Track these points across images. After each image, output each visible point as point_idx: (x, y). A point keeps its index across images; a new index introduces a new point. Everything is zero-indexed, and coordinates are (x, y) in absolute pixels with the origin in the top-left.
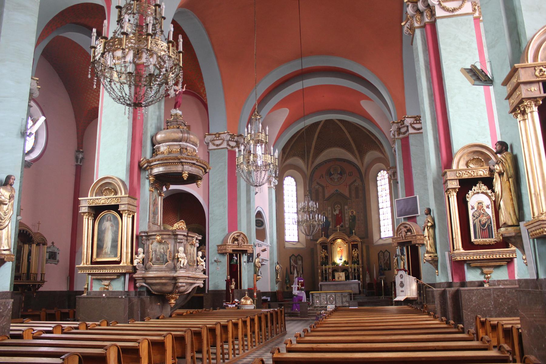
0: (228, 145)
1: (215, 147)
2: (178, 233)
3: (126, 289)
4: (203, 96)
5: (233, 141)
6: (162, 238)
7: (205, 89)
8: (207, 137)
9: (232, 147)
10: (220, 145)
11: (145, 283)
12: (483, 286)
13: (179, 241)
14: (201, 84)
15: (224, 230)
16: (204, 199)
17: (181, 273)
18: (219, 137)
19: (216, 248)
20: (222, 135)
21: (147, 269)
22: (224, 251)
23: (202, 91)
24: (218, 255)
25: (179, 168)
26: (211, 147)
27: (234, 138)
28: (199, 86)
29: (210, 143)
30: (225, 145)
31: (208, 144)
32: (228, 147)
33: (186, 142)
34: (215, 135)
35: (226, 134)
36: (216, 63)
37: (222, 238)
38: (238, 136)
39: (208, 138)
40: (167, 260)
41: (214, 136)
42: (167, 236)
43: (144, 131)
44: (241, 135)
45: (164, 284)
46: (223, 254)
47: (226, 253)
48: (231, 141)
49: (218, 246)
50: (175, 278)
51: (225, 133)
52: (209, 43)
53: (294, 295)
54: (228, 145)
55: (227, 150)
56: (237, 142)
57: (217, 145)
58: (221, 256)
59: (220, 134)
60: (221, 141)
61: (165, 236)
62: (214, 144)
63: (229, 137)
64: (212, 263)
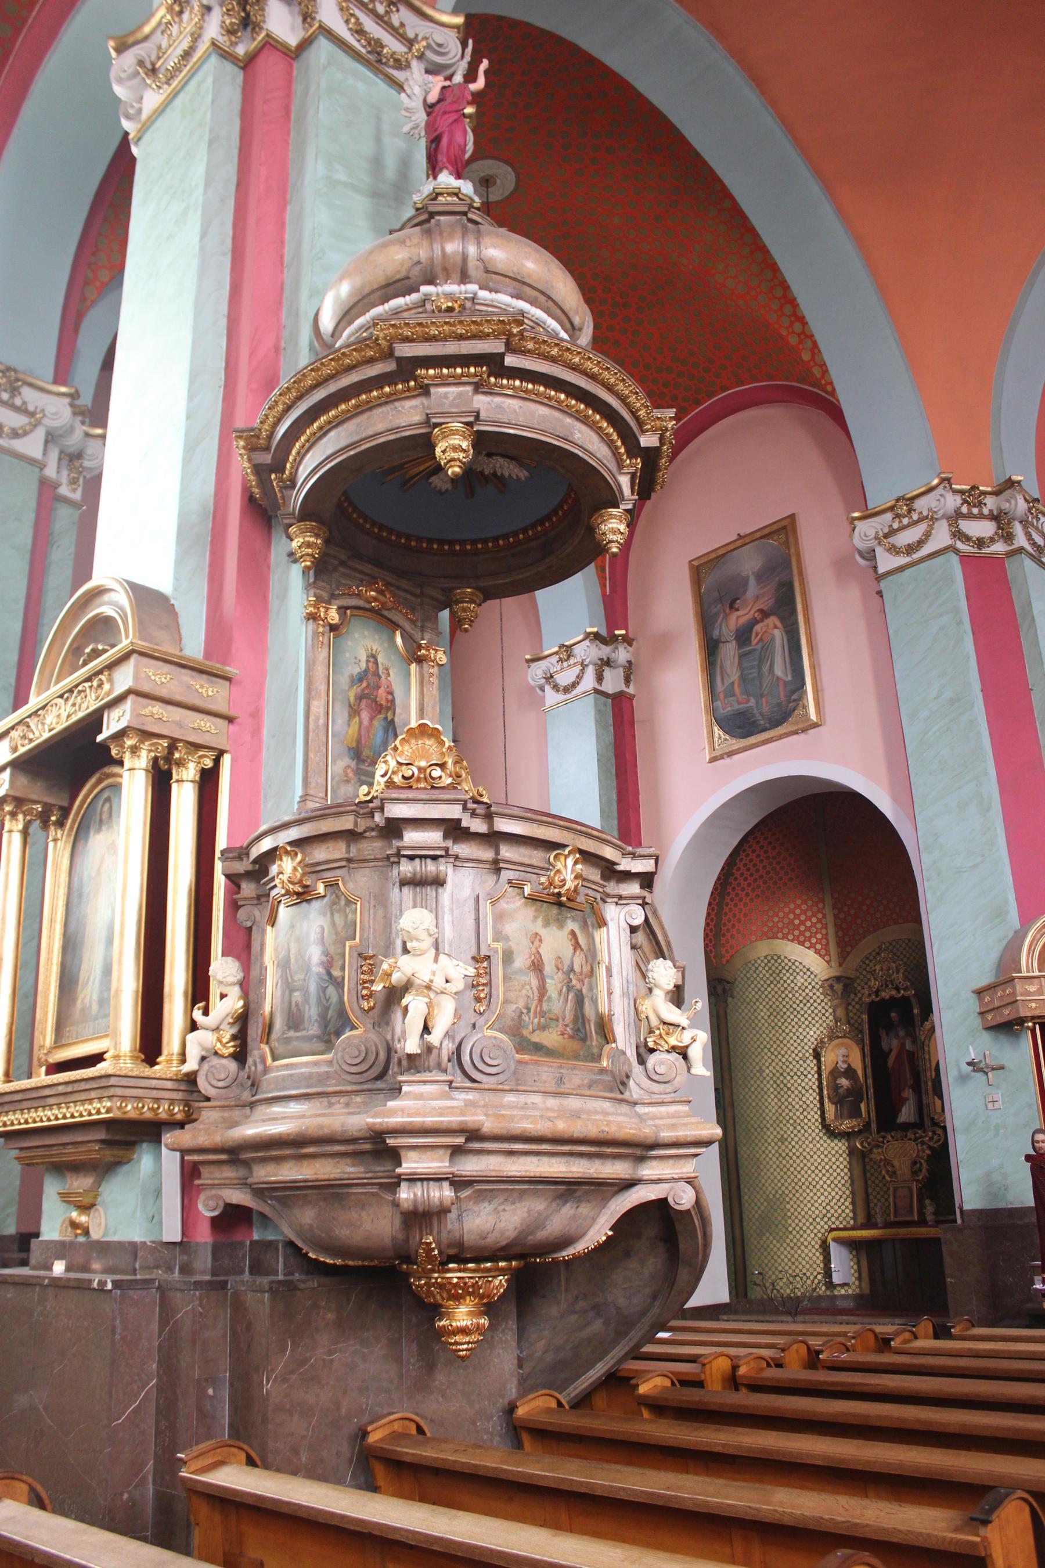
0: (959, 535)
1: (902, 560)
2: (398, 811)
3: (173, 1233)
4: (829, 388)
5: (981, 516)
6: (314, 869)
7: (815, 344)
8: (862, 527)
9: (980, 543)
10: (921, 543)
11: (243, 1184)
12: (51, 1269)
13: (407, 868)
14: (797, 327)
15: (1000, 914)
16: (895, 798)
17: (419, 1102)
18: (910, 511)
19: (973, 1004)
20: (919, 504)
21: (250, 1094)
22: (1007, 1014)
23: (806, 356)
24: (986, 1037)
25: (404, 415)
26: (886, 562)
27: (980, 504)
28: (793, 340)
29: (879, 551)
30: (941, 537)
31: (870, 556)
32: (960, 545)
33: (464, 278)
34: (891, 509)
35: (940, 490)
36: (827, 209)
37: (994, 956)
38: (996, 494)
39: (867, 530)
40: (342, 1013)
41: (889, 516)
42: (336, 851)
43: (285, 333)
44: (1010, 484)
45: (330, 1192)
46: (1008, 1027)
47: (1021, 1021)
48: (970, 516)
49: (979, 993)
50: (380, 1148)
51: (931, 489)
52: (768, 121)
53: (591, 530)
54: (959, 535)
55: (954, 559)
56: (995, 517)
57: (910, 549)
58: (1004, 1039)
59: (913, 499)
60: (922, 527)
61: (321, 853)
62: (894, 550)
63: (952, 502)
64: (963, 1079)
